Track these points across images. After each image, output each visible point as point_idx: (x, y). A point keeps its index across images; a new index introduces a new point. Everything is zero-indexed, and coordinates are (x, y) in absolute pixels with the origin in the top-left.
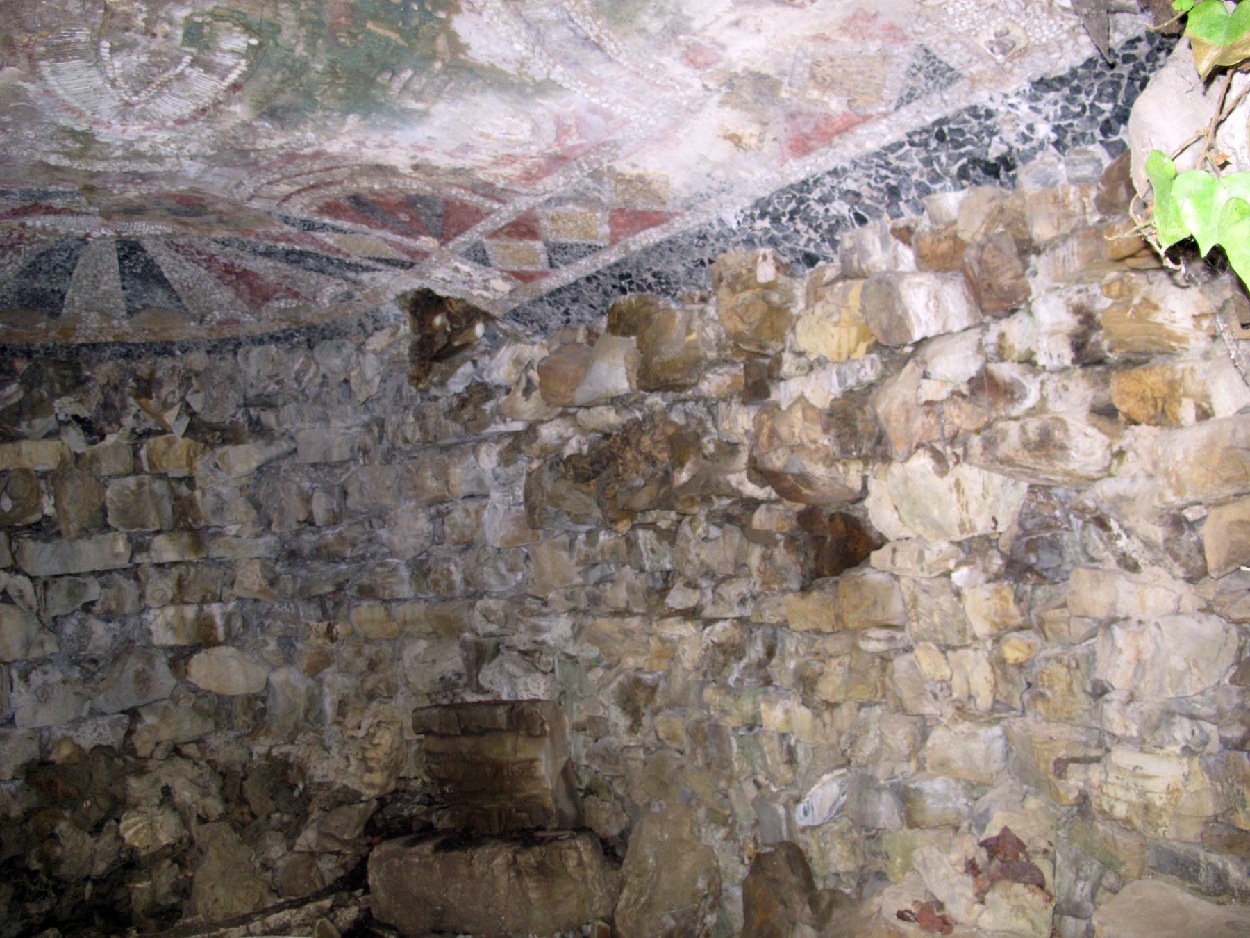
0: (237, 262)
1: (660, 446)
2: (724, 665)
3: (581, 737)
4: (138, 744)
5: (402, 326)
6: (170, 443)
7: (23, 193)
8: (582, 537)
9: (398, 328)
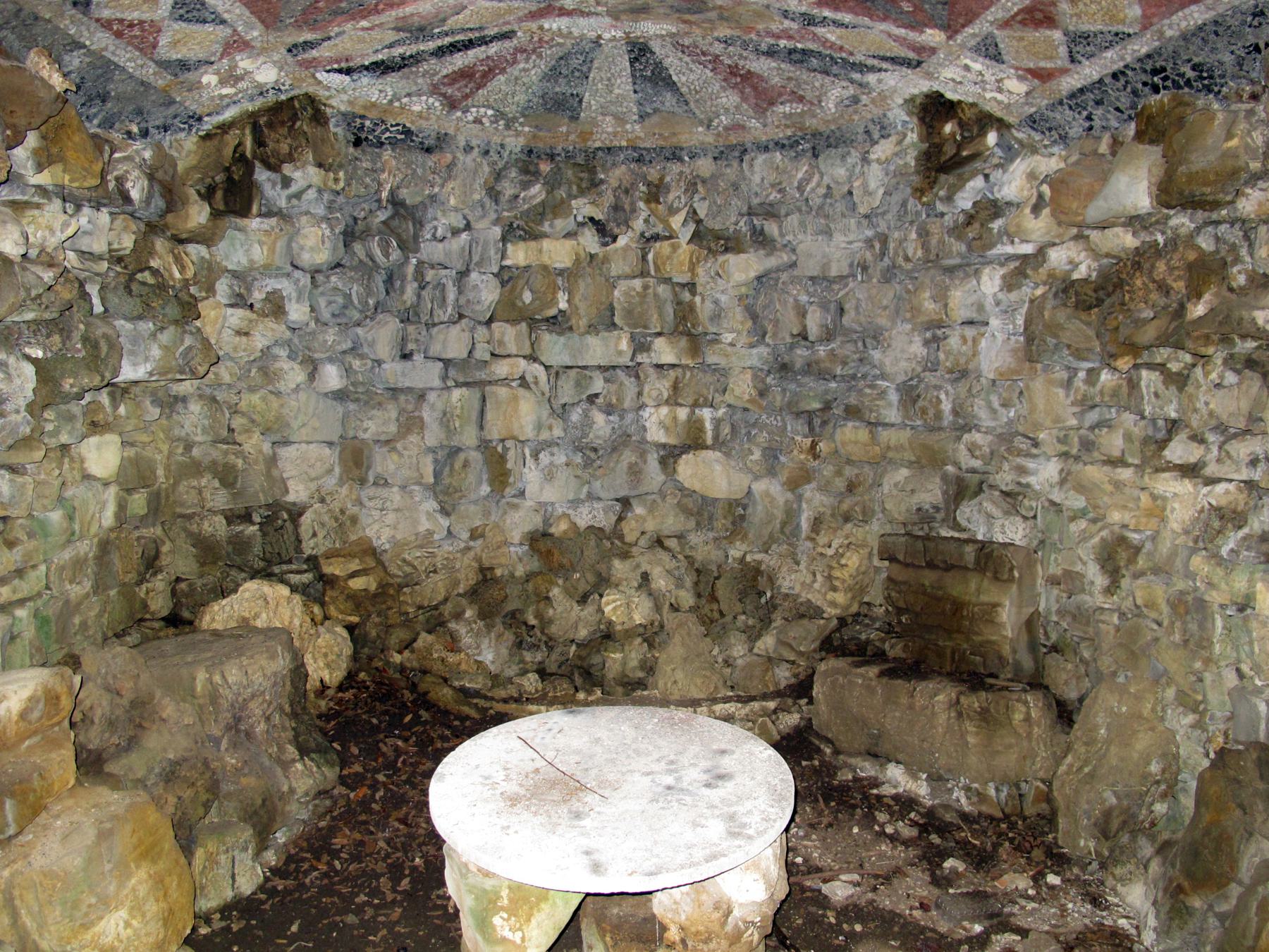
0: (741, 63)
1: (1177, 273)
2: (1219, 532)
3: (1055, 592)
4: (626, 531)
5: (909, 134)
6: (675, 248)
8: (1082, 375)
9: (905, 136)
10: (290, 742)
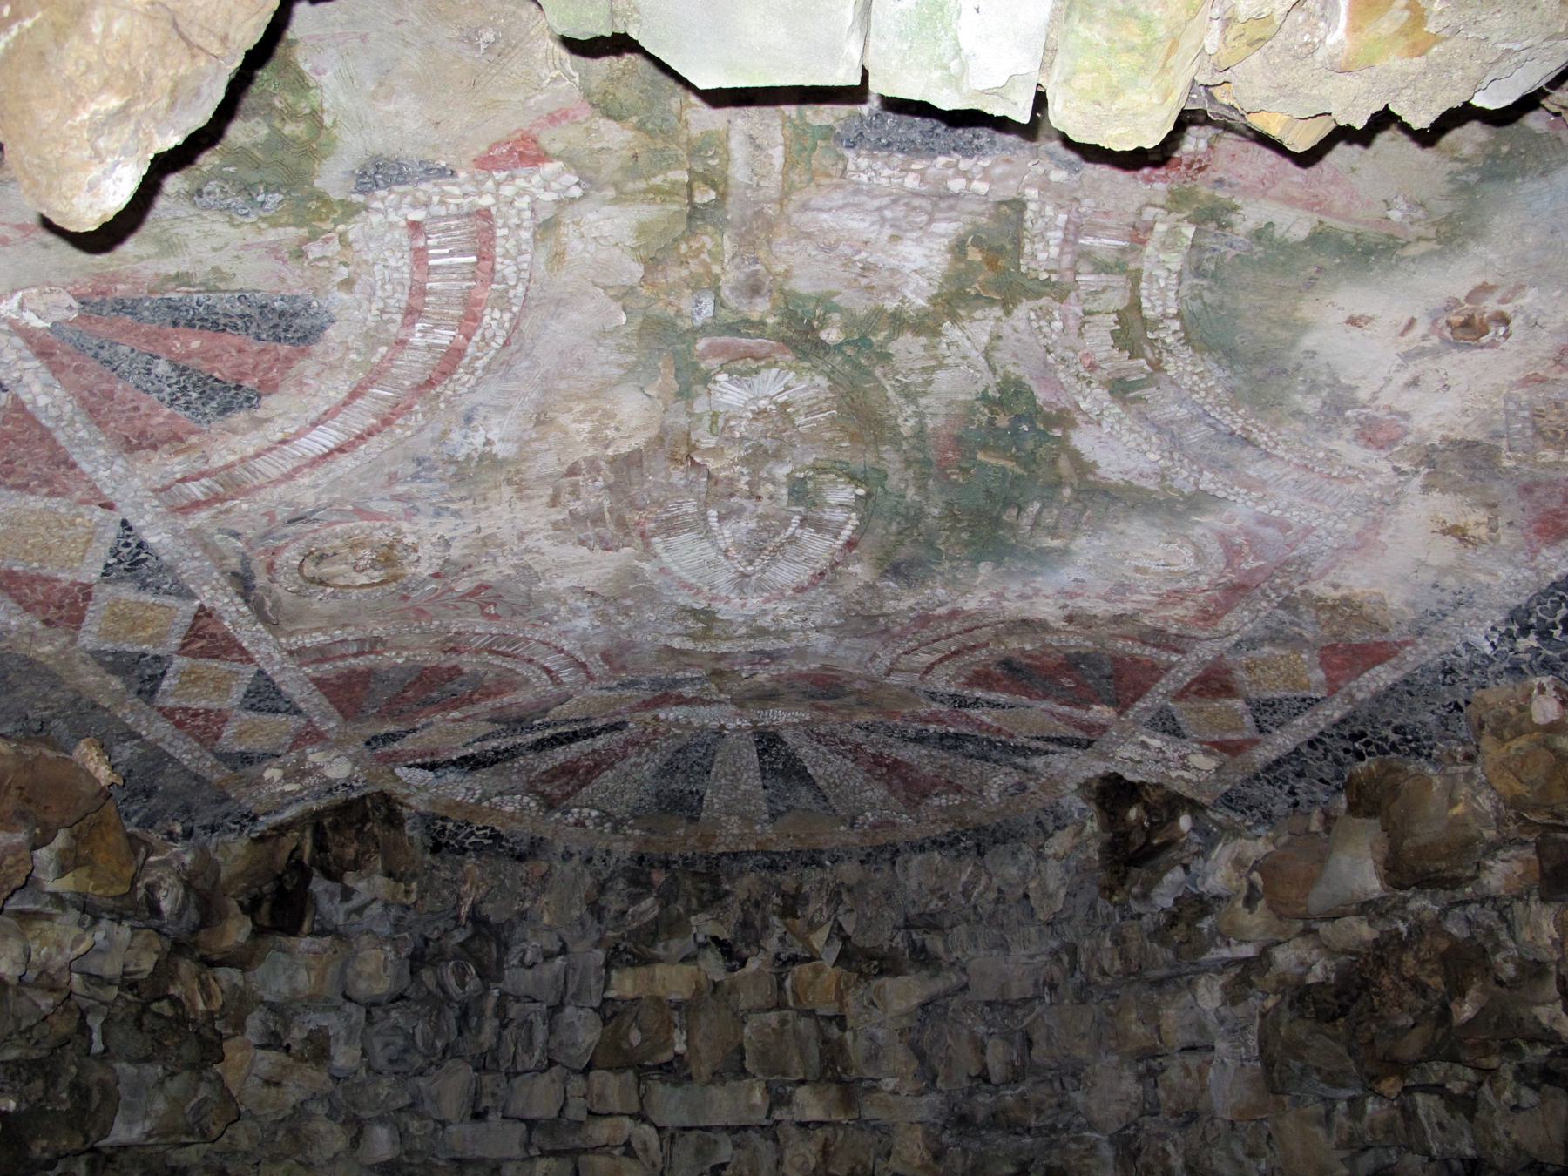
0: (886, 751)
1: (1429, 967)
5: (1089, 823)
6: (818, 971)
7: (653, 682)
8: (1342, 1106)
9: (1084, 825)
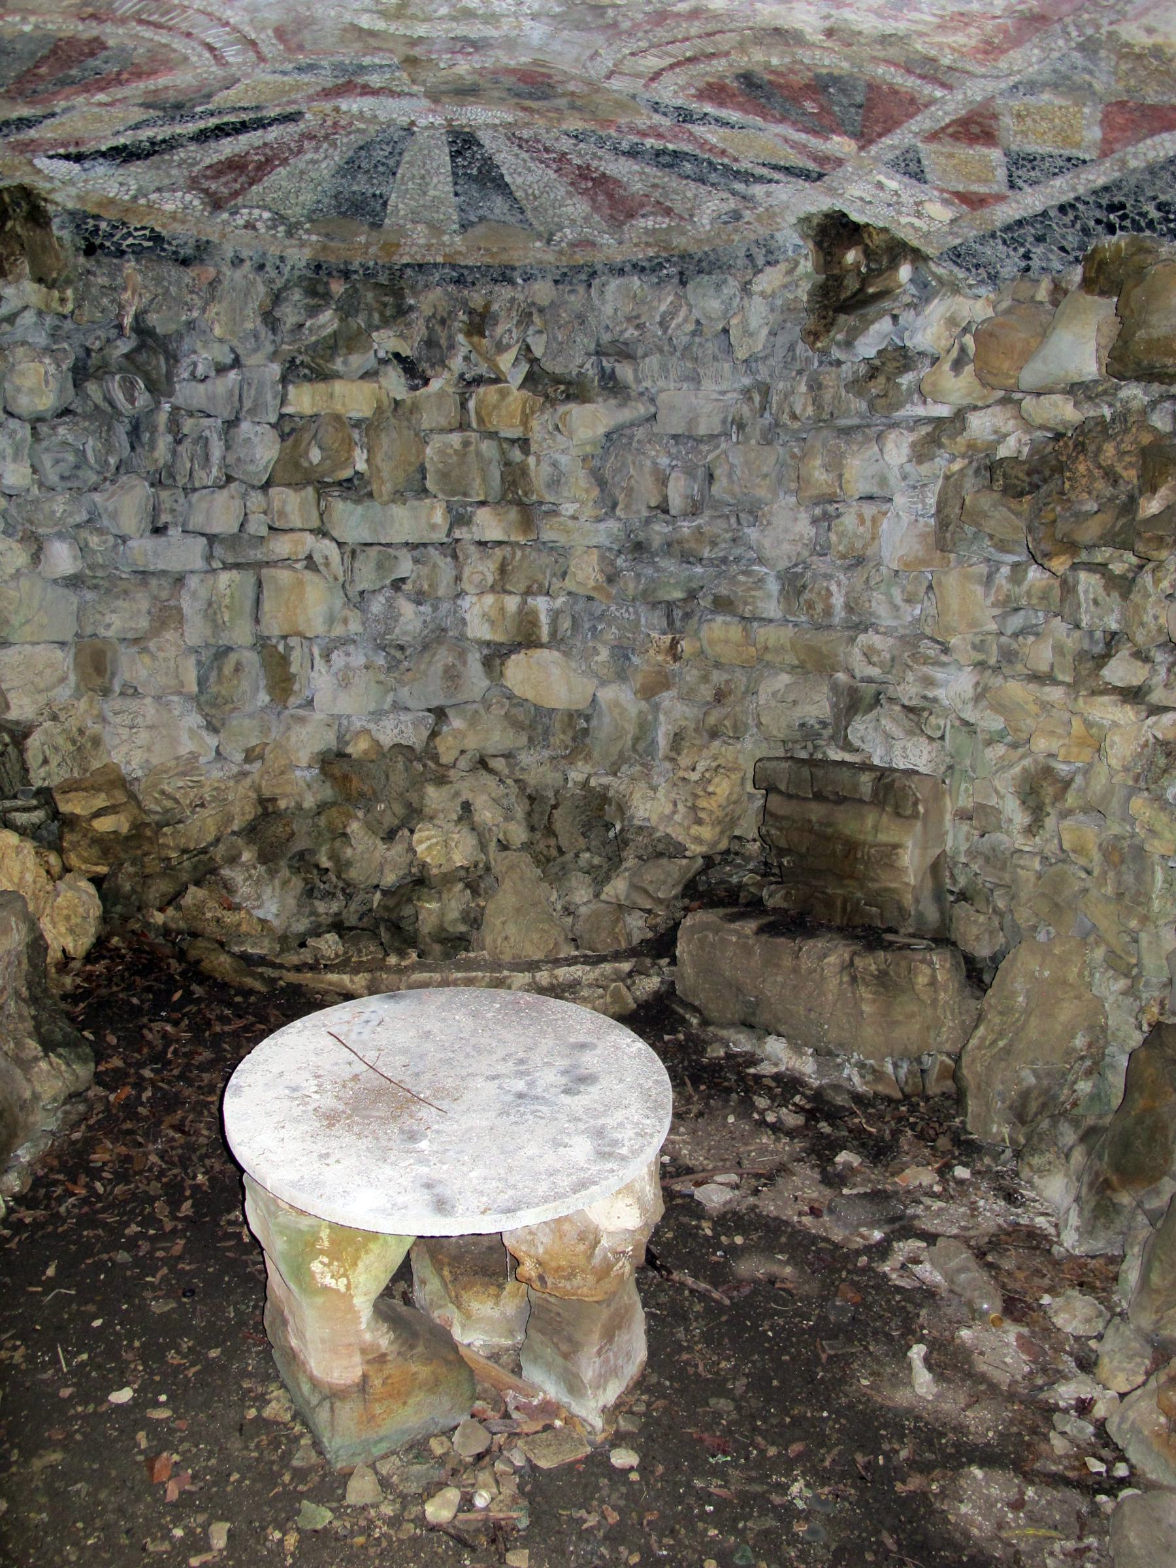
0: (595, 163)
1: (1128, 459)
2: (1165, 771)
3: (965, 827)
4: (441, 749)
5: (802, 261)
6: (504, 394)
8: (1005, 570)
9: (797, 264)
10: (30, 1035)
